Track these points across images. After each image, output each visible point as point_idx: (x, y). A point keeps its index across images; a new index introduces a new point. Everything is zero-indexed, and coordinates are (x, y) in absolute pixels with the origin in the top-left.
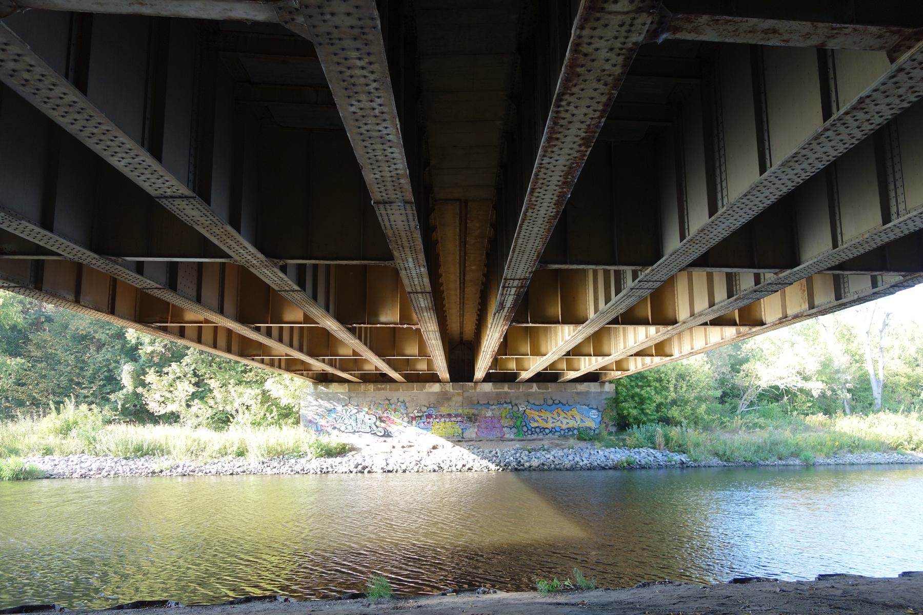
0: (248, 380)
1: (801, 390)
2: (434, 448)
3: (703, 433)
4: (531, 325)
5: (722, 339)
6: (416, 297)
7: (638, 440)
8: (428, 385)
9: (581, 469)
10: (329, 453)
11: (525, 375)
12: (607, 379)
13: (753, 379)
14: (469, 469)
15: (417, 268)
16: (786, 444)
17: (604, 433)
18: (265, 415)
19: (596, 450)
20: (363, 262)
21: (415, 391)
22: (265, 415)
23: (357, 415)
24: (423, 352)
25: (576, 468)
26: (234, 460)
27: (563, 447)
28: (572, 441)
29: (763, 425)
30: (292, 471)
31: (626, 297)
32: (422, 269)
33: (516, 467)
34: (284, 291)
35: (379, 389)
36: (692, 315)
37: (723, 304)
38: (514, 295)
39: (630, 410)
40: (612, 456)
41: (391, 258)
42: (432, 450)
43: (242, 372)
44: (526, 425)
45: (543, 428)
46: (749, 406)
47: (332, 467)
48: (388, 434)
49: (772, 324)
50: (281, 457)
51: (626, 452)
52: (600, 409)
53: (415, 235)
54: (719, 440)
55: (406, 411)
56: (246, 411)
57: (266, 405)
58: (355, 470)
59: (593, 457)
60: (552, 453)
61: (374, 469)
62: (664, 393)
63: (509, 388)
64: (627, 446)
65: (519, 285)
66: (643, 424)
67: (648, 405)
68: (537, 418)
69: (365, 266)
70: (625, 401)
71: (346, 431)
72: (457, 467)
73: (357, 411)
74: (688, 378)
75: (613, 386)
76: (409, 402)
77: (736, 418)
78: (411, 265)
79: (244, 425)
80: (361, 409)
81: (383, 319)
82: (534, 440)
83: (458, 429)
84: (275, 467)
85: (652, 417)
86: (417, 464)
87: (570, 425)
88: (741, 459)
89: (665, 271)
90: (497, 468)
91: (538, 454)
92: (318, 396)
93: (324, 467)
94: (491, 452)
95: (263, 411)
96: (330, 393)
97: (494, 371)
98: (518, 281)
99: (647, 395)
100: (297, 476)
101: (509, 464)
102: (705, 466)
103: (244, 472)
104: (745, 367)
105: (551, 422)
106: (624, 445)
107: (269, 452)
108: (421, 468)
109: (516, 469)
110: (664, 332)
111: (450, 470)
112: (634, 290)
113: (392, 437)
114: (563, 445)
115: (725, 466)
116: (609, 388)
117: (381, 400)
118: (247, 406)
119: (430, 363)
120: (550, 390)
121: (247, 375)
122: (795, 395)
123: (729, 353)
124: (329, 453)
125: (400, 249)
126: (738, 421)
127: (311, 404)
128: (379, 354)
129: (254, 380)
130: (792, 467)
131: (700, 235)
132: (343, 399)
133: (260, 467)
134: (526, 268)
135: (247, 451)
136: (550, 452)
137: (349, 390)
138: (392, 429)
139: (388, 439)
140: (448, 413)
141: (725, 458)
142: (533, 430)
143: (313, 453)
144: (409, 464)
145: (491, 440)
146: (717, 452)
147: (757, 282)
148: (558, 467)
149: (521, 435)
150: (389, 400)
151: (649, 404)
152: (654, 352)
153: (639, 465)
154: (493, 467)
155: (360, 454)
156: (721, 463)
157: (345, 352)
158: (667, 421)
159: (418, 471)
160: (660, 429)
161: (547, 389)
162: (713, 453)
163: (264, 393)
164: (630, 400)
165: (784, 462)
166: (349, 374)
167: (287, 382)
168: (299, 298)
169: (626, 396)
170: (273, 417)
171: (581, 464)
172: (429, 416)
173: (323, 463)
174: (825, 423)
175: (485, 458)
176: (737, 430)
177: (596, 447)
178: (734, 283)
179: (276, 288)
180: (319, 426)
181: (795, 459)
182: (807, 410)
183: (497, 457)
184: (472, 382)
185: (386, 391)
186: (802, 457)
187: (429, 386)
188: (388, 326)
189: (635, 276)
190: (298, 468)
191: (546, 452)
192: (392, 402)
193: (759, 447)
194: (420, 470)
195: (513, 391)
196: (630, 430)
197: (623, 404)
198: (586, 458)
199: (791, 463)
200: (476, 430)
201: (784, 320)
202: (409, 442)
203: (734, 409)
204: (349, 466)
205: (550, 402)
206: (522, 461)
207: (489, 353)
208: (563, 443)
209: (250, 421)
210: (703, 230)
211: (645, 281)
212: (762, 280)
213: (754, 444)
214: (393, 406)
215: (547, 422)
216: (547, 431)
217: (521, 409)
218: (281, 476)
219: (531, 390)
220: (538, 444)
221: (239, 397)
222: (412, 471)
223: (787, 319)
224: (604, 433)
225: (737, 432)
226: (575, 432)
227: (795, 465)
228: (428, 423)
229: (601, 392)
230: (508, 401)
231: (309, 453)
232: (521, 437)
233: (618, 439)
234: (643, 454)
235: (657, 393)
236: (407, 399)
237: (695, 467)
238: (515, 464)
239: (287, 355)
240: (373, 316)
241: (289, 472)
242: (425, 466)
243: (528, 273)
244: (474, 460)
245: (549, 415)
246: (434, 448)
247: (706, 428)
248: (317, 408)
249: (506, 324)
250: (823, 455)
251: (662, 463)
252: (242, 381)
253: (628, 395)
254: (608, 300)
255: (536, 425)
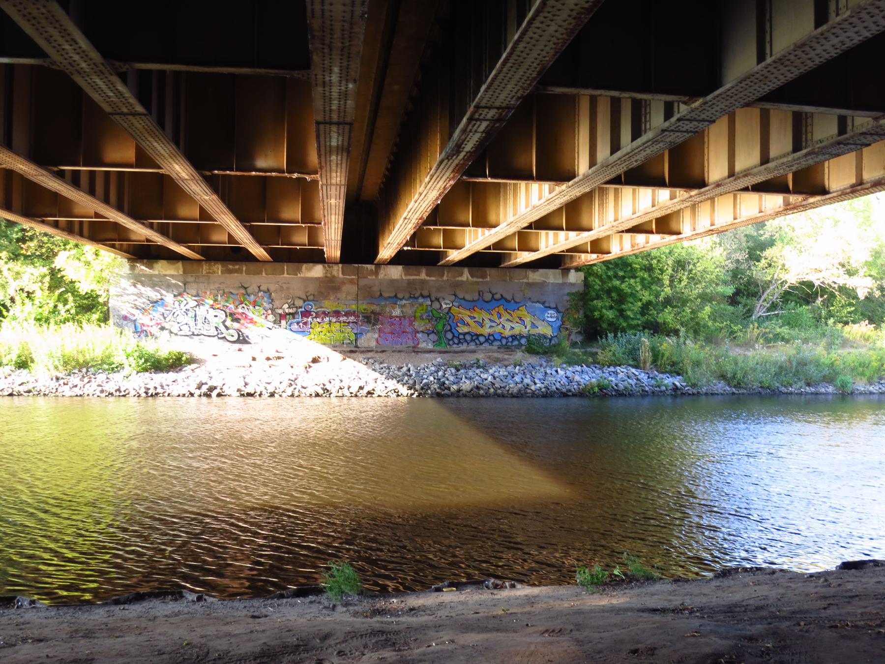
0: (29, 253)
1: (843, 289)
2: (315, 361)
3: (705, 346)
4: (490, 180)
5: (761, 212)
6: (327, 130)
7: (614, 354)
8: (304, 266)
9: (534, 395)
10: (157, 366)
11: (455, 256)
12: (575, 264)
13: (778, 271)
14: (369, 393)
15: (344, 82)
16: (817, 363)
17: (566, 344)
18: (56, 306)
19: (554, 369)
20: (258, 70)
21: (285, 275)
22: (56, 306)
23: (197, 309)
24: (308, 216)
25: (526, 393)
26: (13, 374)
27: (506, 363)
28: (519, 355)
29: (787, 337)
30: (102, 391)
31: (650, 143)
32: (351, 86)
33: (438, 390)
34: (119, 114)
35: (230, 272)
36: (732, 174)
37: (785, 160)
38: (483, 132)
39: (604, 311)
40: (577, 378)
41: (305, 64)
42: (311, 364)
43: (18, 240)
44: (450, 330)
45: (476, 335)
46: (768, 310)
47: (162, 387)
48: (244, 339)
49: (839, 193)
50: (84, 370)
51: (598, 371)
52: (560, 309)
53: (356, 29)
54: (727, 356)
55: (271, 306)
56: (27, 301)
57: (57, 292)
58: (197, 392)
59: (550, 379)
60: (491, 371)
61: (227, 391)
62: (654, 287)
63: (427, 275)
64: (598, 363)
65: (495, 118)
66: (621, 332)
67: (630, 305)
68: (468, 319)
69: (232, 76)
70: (598, 297)
71: (179, 333)
72: (351, 390)
73: (196, 303)
74: (691, 266)
75: (581, 275)
76: (275, 291)
77: (751, 326)
78: (335, 78)
79: (25, 322)
80: (203, 301)
81: (261, 163)
82: (462, 352)
83: (349, 332)
84: (76, 386)
85: (635, 322)
86: (291, 385)
87: (516, 331)
88: (756, 385)
89: (722, 106)
90: (410, 392)
91: (471, 373)
92: (137, 280)
93: (151, 386)
94: (400, 368)
95: (52, 301)
96: (155, 276)
97: (409, 248)
98: (495, 110)
99: (629, 291)
100: (111, 399)
101: (427, 386)
102: (706, 394)
103: (29, 391)
104: (768, 253)
105: (488, 326)
106: (595, 362)
107: (66, 363)
108: (297, 391)
109: (439, 395)
110: (682, 198)
111: (340, 394)
112: (666, 133)
113: (249, 343)
114: (505, 360)
115: (733, 393)
116: (574, 277)
117: (233, 288)
118: (28, 292)
119: (313, 235)
120: (488, 279)
121: (26, 245)
122: (832, 296)
123: (747, 233)
124: (157, 366)
125: (326, 51)
126: (753, 330)
127: (126, 292)
128: (242, 217)
129: (38, 253)
130: (823, 396)
131: (796, 53)
132: (176, 285)
133: (53, 384)
134: (515, 90)
135: (32, 361)
136: (487, 371)
137: (184, 272)
138: (249, 331)
139: (244, 347)
140: (334, 309)
141: (735, 382)
142: (461, 337)
143: (133, 365)
144: (278, 385)
145: (399, 351)
146: (725, 373)
147: (842, 130)
148: (499, 391)
149: (443, 345)
150: (246, 288)
151: (632, 303)
152: (654, 227)
153: (615, 390)
154: (404, 390)
155: (203, 368)
156: (729, 389)
157: (188, 214)
158: (656, 328)
159: (292, 396)
160: (646, 340)
161: (484, 277)
162: (719, 374)
163: (53, 273)
164: (605, 297)
165: (813, 390)
166: (185, 247)
167: (90, 256)
168: (139, 126)
169: (599, 290)
170: (68, 311)
171: (533, 388)
172: (306, 314)
173: (148, 381)
174: (869, 337)
175: (393, 378)
176: (752, 342)
177: (553, 364)
178: (804, 129)
179: (107, 108)
180: (138, 325)
181: (827, 385)
182: (846, 317)
183: (411, 376)
184: (371, 263)
185: (241, 276)
186: (838, 383)
187: (306, 269)
188: (269, 174)
189: (669, 113)
190: (111, 387)
191: (481, 370)
192: (250, 290)
193: (781, 367)
194: (296, 394)
195: (433, 278)
196: (604, 340)
197: (595, 302)
198: (540, 380)
199: (823, 390)
200: (376, 336)
201: (859, 188)
202: (277, 352)
203: (749, 313)
204: (188, 385)
205: (488, 297)
206: (447, 382)
207: (413, 221)
208: (506, 357)
209: (33, 316)
210: (803, 45)
211: (688, 120)
212: (849, 128)
213: (775, 363)
214: (252, 298)
215: (482, 326)
216: (482, 339)
217: (444, 306)
218: (86, 398)
219: (460, 279)
220: (471, 358)
221: (15, 279)
222: (284, 394)
223: (864, 186)
224: (566, 344)
225: (753, 347)
226: (523, 341)
227: (827, 394)
228: (305, 323)
229: (564, 284)
230: (426, 293)
231: (126, 366)
232: (443, 347)
233: (585, 353)
234: (621, 375)
235: (644, 287)
236: (272, 288)
237: (693, 394)
238: (436, 386)
239: (97, 215)
240: (246, 161)
241: (98, 393)
242: (303, 387)
243: (514, 99)
244: (376, 380)
245: (486, 316)
246: (315, 361)
247: (711, 339)
248: (136, 298)
249: (453, 178)
250: (865, 379)
251: (647, 389)
252: (19, 255)
253: (602, 290)
254: (615, 147)
255: (465, 329)
